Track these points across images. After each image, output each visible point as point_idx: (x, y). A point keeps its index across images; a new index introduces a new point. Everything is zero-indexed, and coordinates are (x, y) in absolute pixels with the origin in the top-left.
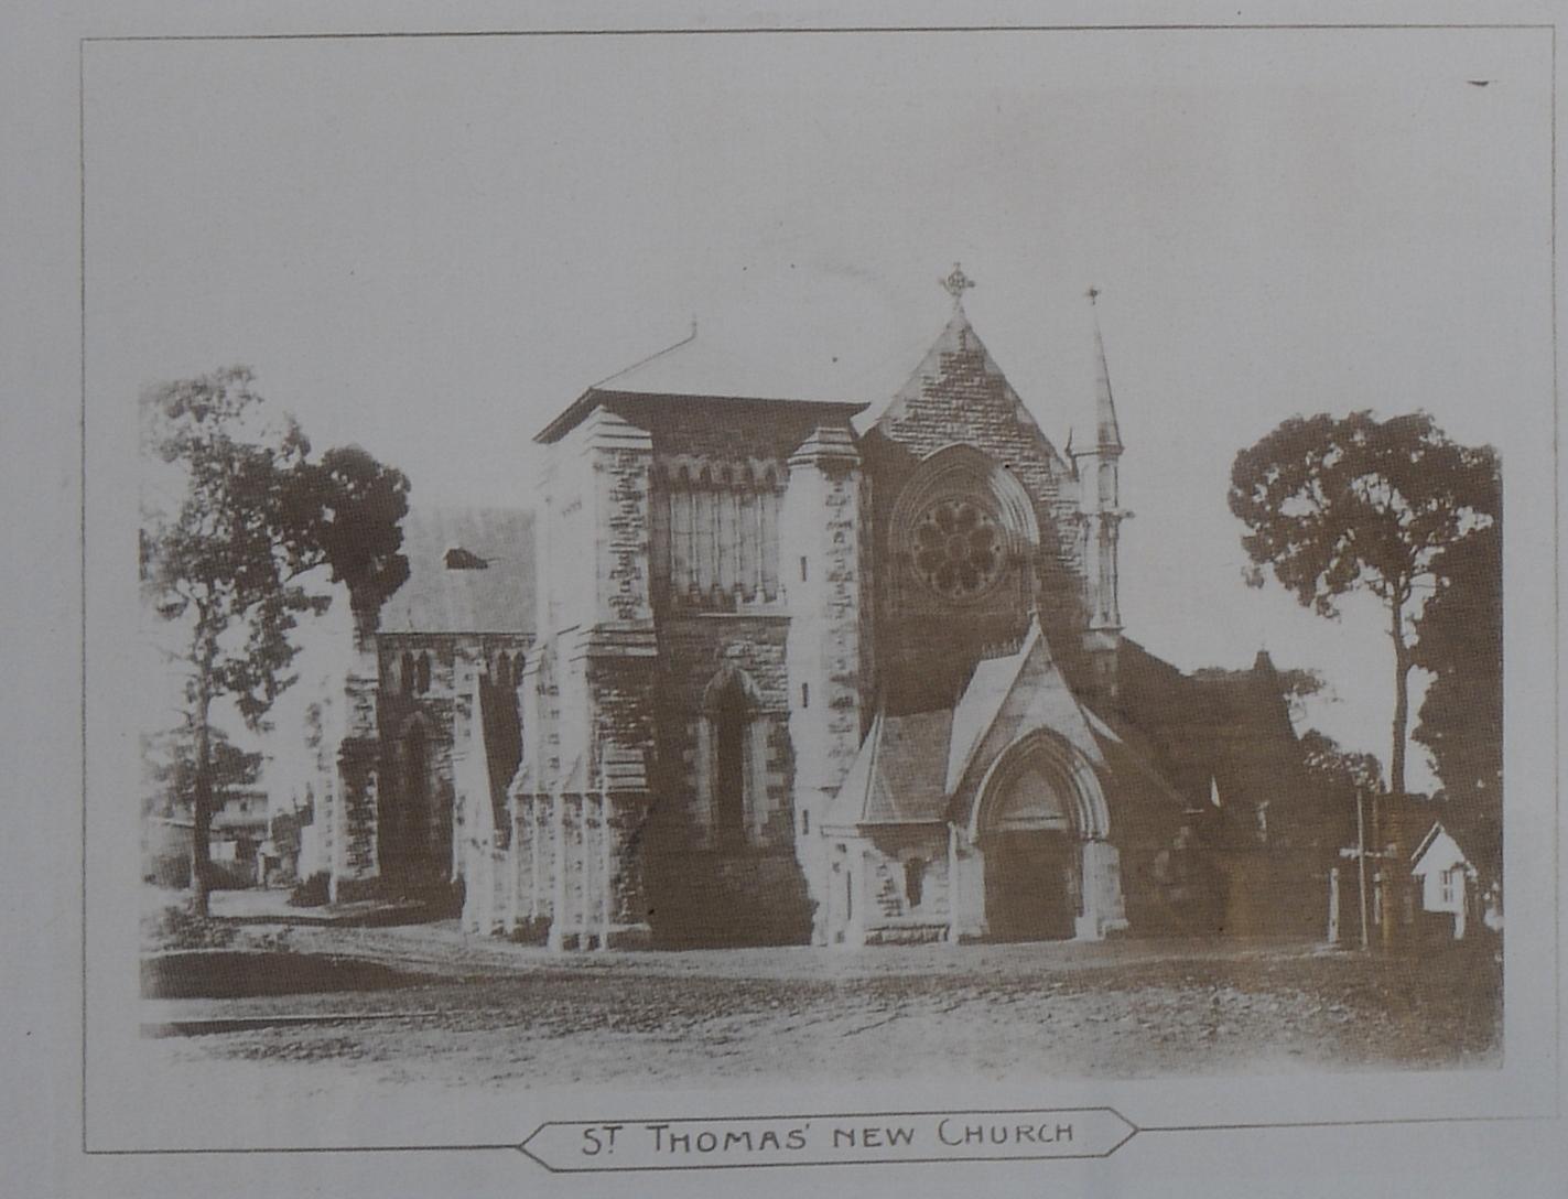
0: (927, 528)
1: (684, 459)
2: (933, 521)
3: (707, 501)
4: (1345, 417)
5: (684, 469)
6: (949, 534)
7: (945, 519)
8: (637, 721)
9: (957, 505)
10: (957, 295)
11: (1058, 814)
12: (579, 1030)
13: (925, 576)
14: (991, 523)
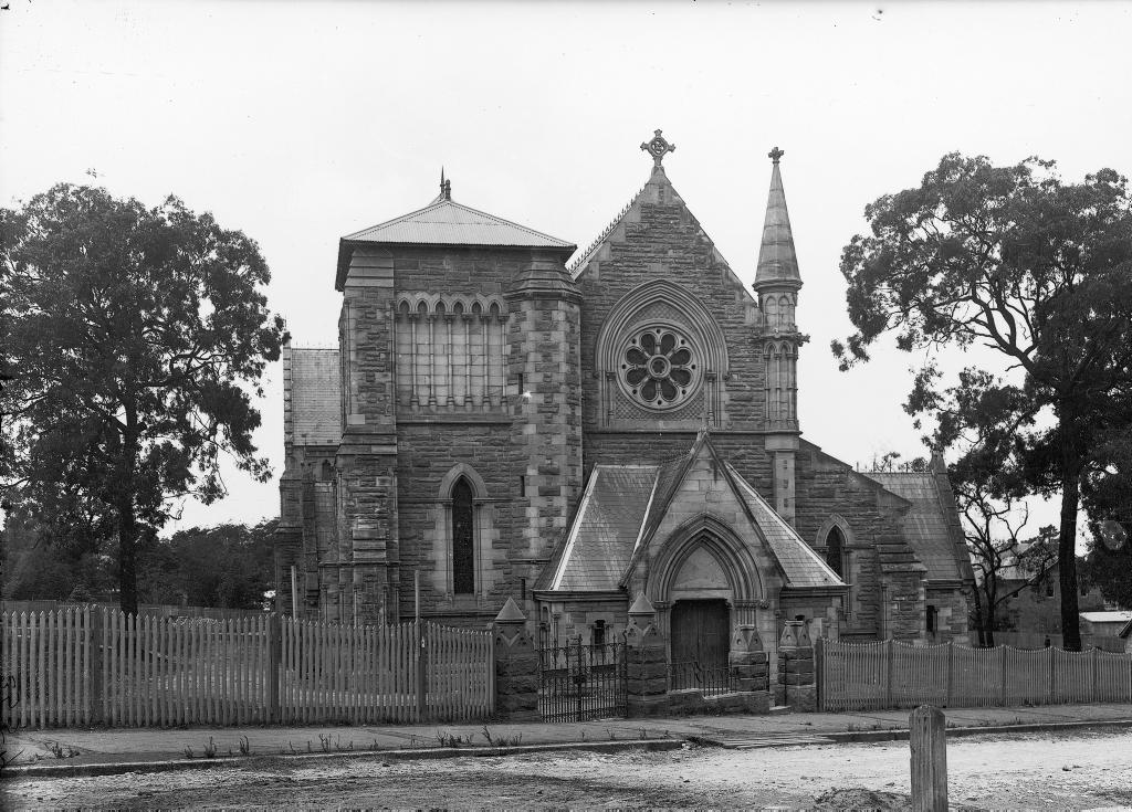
0: (633, 351)
1: (419, 296)
2: (637, 345)
3: (442, 329)
4: (1069, 185)
5: (422, 304)
6: (652, 354)
7: (648, 341)
8: (106, 528)
9: (658, 332)
10: (658, 158)
11: (724, 586)
12: (633, 568)
13: (630, 389)
14: (687, 345)
